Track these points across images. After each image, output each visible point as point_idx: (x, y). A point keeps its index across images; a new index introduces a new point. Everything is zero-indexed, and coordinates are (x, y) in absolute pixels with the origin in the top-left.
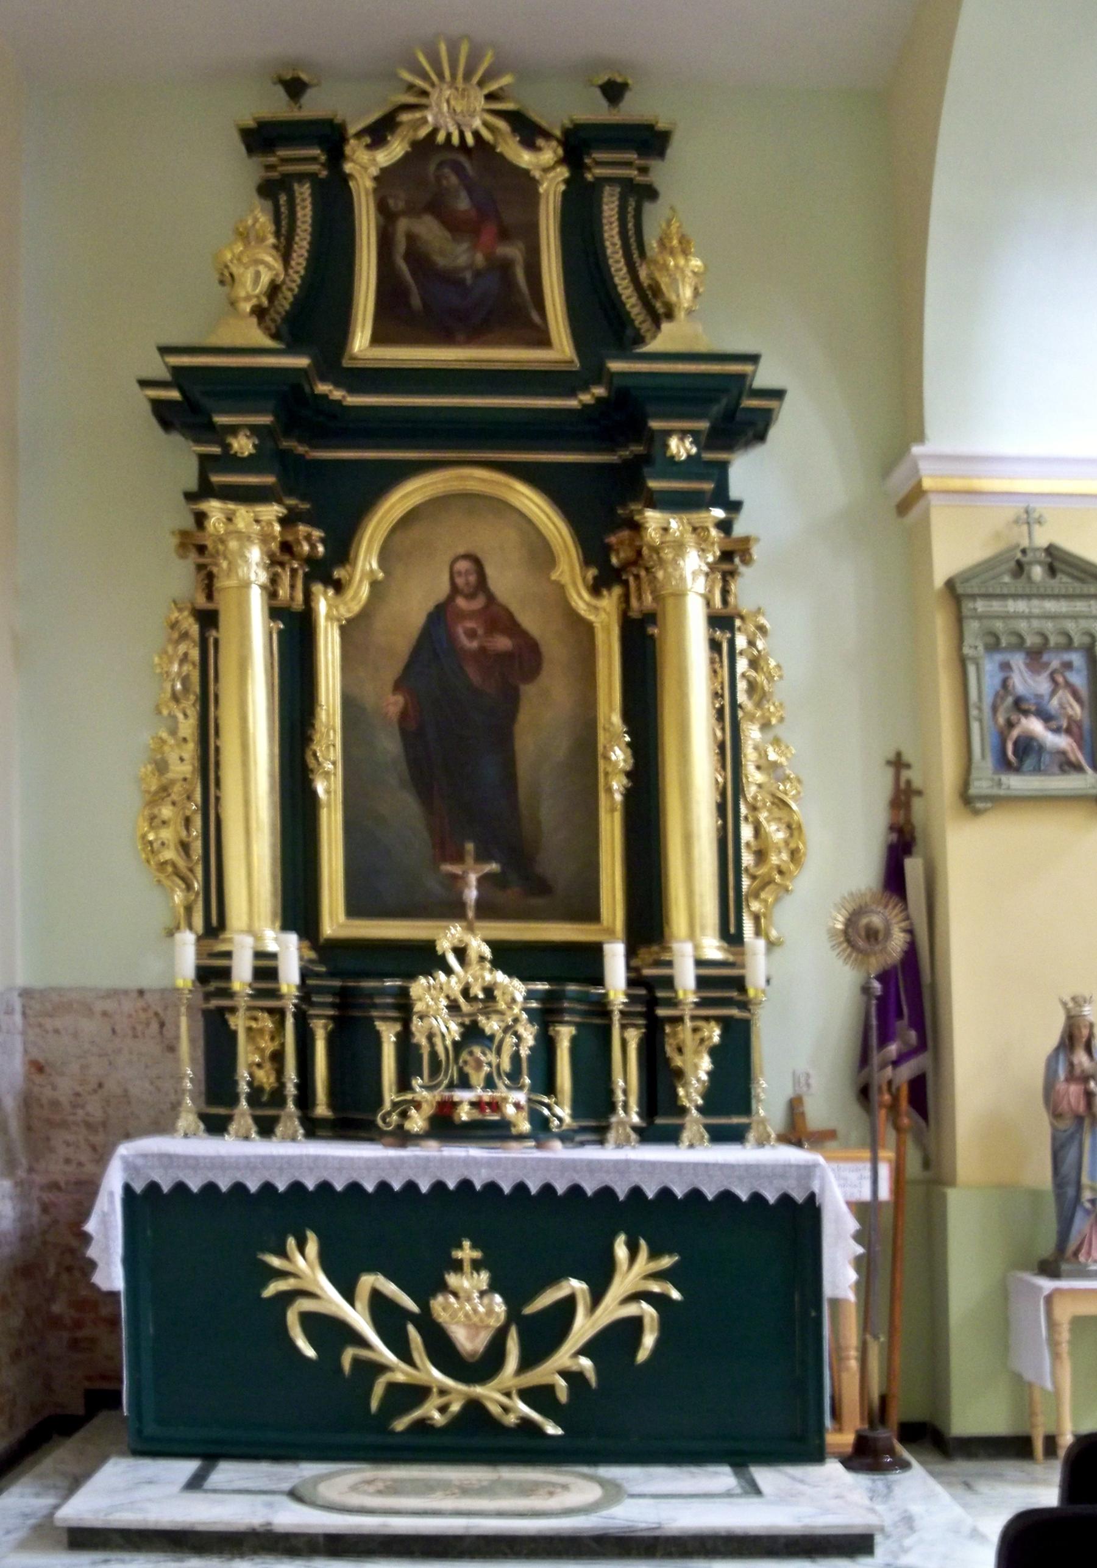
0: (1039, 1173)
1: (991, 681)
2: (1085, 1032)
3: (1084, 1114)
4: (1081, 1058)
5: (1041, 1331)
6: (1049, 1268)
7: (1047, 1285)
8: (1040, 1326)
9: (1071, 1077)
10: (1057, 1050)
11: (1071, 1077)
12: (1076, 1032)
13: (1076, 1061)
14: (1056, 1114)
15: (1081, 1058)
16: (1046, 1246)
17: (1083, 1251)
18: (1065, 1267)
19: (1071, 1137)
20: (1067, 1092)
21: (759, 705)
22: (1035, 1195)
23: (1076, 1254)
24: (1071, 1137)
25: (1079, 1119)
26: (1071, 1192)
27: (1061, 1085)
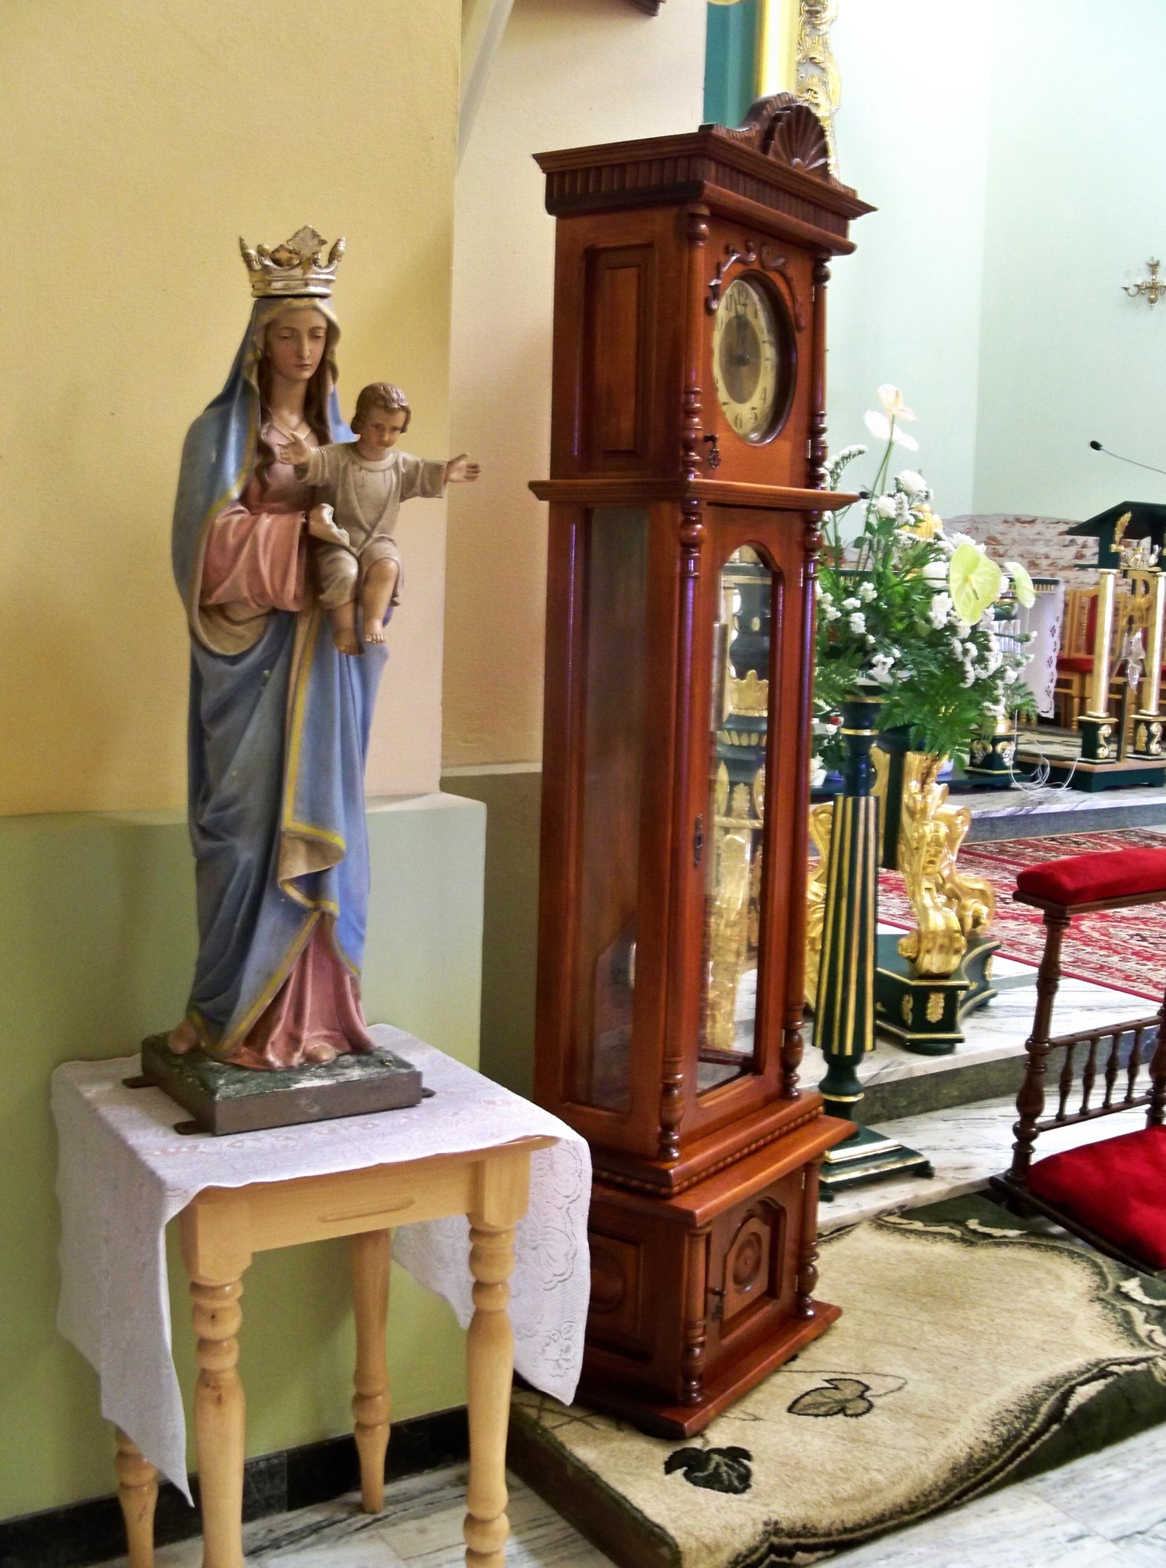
0: (153, 778)
1: (914, 867)
2: (312, 351)
3: (293, 608)
4: (288, 429)
5: (160, 1333)
6: (188, 1080)
7: (187, 1165)
8: (160, 1323)
9: (258, 497)
10: (223, 401)
11: (258, 497)
12: (282, 349)
13: (276, 440)
14: (210, 611)
15: (288, 429)
16: (165, 1007)
17: (278, 1032)
18: (226, 1088)
19: (254, 679)
20: (247, 535)
21: (859, 747)
22: (137, 840)
23: (258, 1036)
24: (254, 679)
25: (281, 622)
26: (246, 851)
27: (229, 517)
